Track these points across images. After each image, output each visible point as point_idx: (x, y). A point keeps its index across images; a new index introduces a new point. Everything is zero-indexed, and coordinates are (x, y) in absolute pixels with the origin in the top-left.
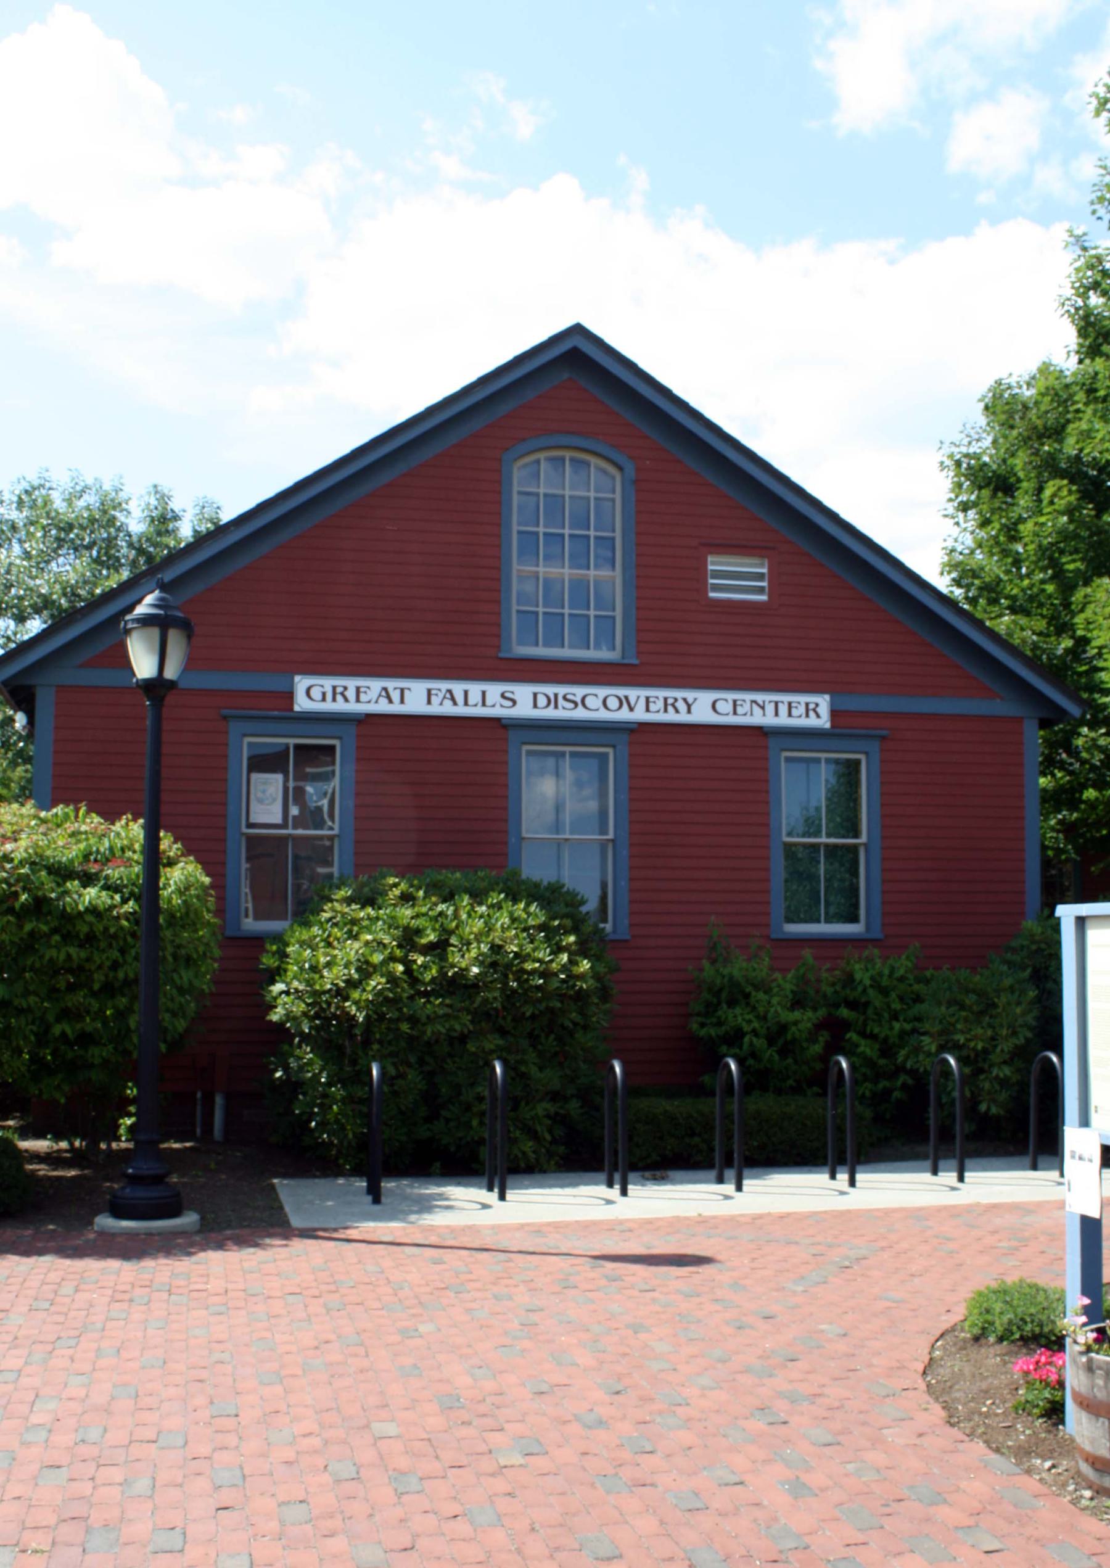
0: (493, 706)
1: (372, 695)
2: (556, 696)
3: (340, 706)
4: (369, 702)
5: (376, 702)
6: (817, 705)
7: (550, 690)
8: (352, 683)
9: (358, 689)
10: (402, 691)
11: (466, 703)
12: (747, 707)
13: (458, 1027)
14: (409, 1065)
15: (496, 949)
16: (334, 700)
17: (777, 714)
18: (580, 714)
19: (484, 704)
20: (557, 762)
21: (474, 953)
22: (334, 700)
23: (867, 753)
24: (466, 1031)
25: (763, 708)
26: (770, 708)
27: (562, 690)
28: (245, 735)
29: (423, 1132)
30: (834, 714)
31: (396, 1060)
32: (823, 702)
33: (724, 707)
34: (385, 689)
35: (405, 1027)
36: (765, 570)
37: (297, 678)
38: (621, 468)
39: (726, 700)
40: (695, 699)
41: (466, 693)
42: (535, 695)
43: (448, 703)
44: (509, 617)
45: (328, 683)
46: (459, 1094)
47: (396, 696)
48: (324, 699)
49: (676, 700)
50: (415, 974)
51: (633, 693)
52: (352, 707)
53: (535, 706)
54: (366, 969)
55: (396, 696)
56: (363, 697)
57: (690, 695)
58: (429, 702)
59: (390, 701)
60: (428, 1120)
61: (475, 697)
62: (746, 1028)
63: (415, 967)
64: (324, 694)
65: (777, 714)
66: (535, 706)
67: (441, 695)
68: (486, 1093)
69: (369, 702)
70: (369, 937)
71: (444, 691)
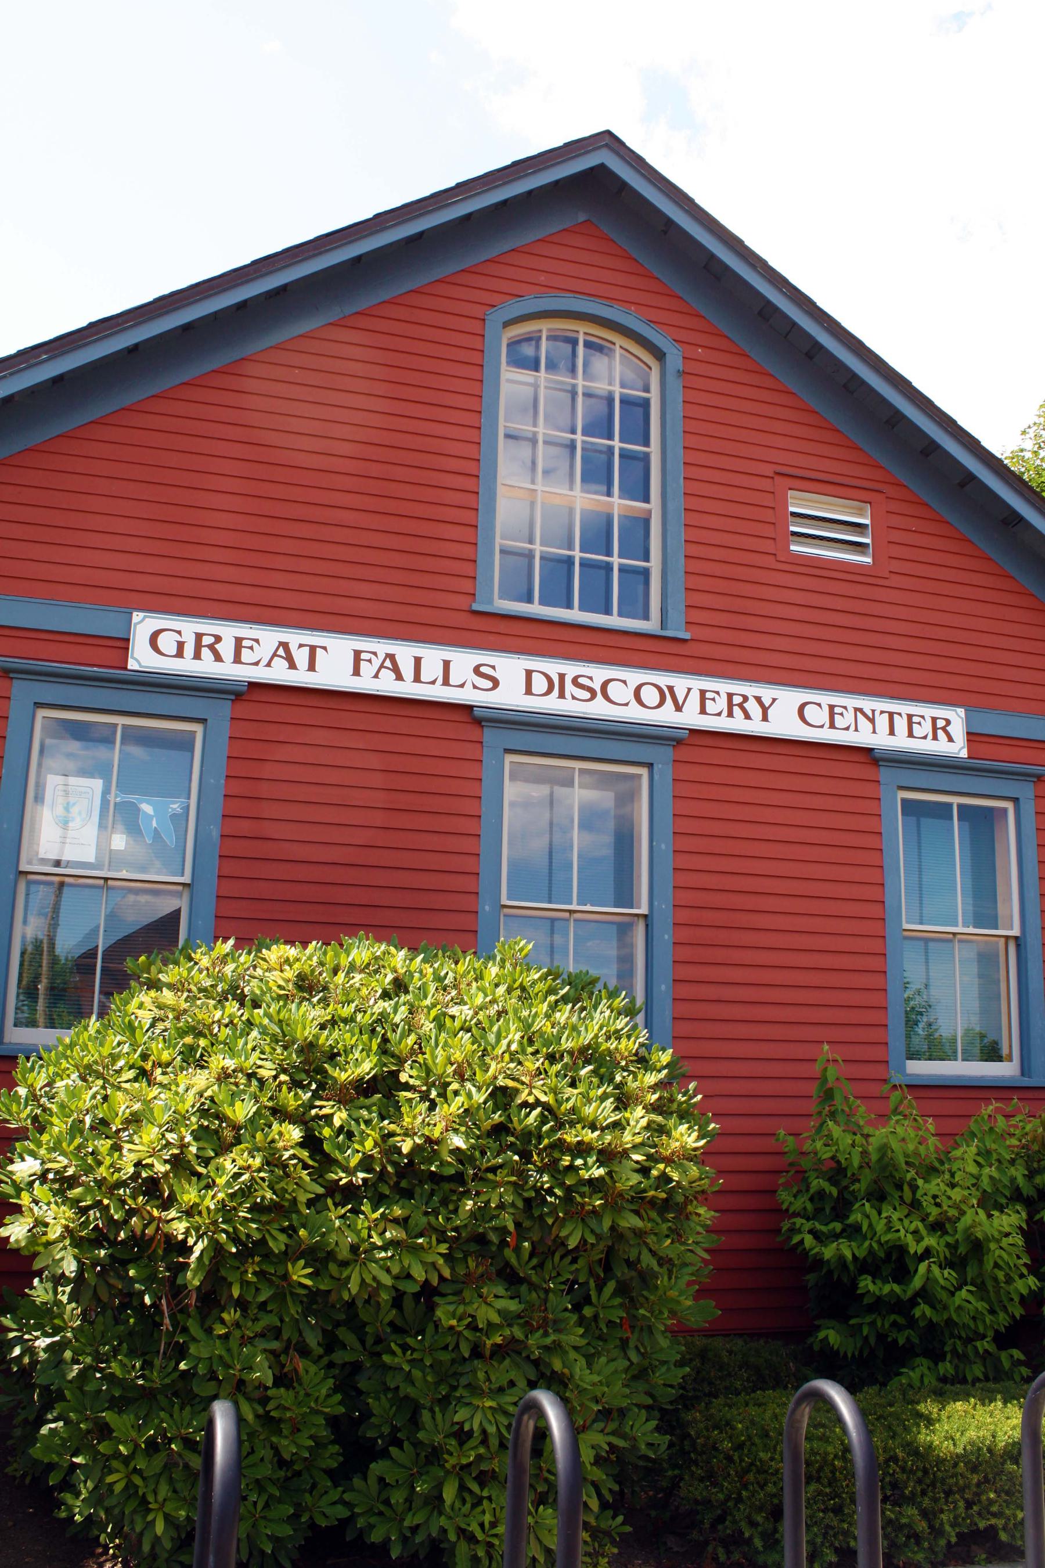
0: (462, 686)
1: (259, 653)
2: (562, 677)
3: (206, 667)
4: (257, 664)
5: (269, 665)
6: (948, 722)
7: (554, 667)
8: (229, 631)
9: (239, 641)
10: (313, 649)
11: (417, 679)
12: (849, 718)
13: (419, 1273)
14: (304, 1352)
15: (502, 1096)
16: (197, 656)
17: (892, 732)
18: (599, 709)
19: (446, 682)
20: (552, 788)
21: (457, 1105)
22: (197, 656)
23: (1015, 800)
24: (435, 1281)
25: (872, 721)
26: (882, 721)
27: (571, 669)
28: (39, 705)
29: (327, 1508)
30: (972, 737)
31: (275, 1345)
32: (957, 718)
33: (817, 715)
34: (285, 645)
35: (300, 1273)
36: (867, 522)
37: (137, 616)
38: (659, 355)
39: (819, 705)
40: (774, 700)
41: (418, 661)
42: (529, 673)
43: (387, 675)
44: (492, 553)
45: (189, 628)
46: (415, 1422)
47: (301, 657)
48: (180, 654)
49: (746, 699)
50: (327, 1147)
51: (681, 683)
52: (228, 670)
53: (529, 691)
54: (216, 1133)
55: (301, 657)
56: (246, 655)
57: (767, 693)
58: (356, 672)
59: (292, 666)
60: (339, 1476)
61: (432, 669)
62: (914, 1247)
63: (327, 1132)
64: (181, 645)
65: (892, 732)
66: (529, 691)
67: (377, 663)
68: (509, 1471)
69: (257, 664)
70: (230, 1064)
71: (381, 656)
